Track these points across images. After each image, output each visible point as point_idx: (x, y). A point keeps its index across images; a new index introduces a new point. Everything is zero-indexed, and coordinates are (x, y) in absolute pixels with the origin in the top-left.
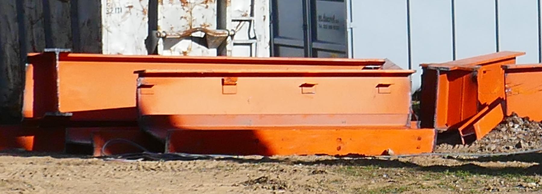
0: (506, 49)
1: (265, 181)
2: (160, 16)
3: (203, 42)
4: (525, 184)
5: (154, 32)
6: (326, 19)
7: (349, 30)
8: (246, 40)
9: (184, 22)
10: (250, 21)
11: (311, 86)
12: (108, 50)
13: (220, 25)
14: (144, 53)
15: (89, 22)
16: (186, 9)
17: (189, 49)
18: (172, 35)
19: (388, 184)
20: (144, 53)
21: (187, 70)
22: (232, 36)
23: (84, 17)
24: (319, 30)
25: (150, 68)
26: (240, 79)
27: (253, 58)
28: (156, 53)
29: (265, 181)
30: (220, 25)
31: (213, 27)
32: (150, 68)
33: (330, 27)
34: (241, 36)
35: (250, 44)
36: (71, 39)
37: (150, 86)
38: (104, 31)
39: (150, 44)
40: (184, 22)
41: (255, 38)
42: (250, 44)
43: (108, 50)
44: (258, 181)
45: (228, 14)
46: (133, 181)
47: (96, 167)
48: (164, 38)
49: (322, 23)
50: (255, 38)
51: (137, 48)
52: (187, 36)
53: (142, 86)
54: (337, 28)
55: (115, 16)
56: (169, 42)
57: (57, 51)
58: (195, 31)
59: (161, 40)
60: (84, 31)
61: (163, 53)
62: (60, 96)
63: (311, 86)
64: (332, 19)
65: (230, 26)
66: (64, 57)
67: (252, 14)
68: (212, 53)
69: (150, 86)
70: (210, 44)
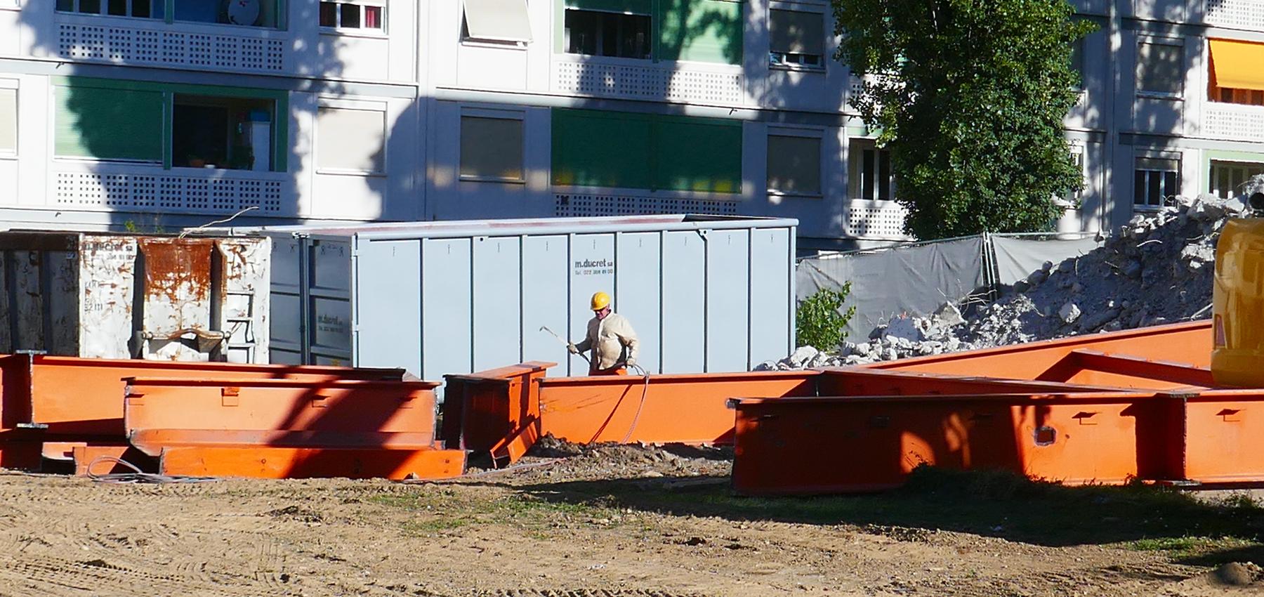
0: (531, 358)
1: (295, 512)
2: (146, 314)
3: (194, 344)
4: (595, 521)
5: (139, 333)
6: (327, 320)
7: (354, 334)
8: (242, 343)
9: (173, 322)
10: (248, 322)
11: (1089, 415)
12: (84, 355)
13: (214, 324)
14: (126, 356)
15: (63, 320)
16: (176, 306)
17: (178, 353)
18: (160, 336)
19: (437, 517)
20: (126, 356)
21: (175, 378)
22: (227, 339)
23: (57, 314)
24: (318, 332)
25: (141, 374)
26: (242, 389)
27: (251, 364)
28: (141, 356)
29: (295, 512)
30: (214, 324)
31: (205, 328)
32: (141, 374)
33: (332, 330)
34: (238, 339)
35: (247, 349)
36: (41, 339)
37: (140, 396)
38: (82, 330)
39: (134, 346)
40: (173, 322)
41: (253, 341)
42: (247, 349)
43: (84, 355)
44: (286, 511)
45: (223, 313)
46: (136, 507)
47: (87, 489)
48: (150, 340)
49: (323, 325)
50: (253, 341)
51: (119, 350)
52: (177, 338)
53: (131, 396)
54: (341, 331)
55: (94, 313)
56: (156, 344)
57: (31, 353)
58: (186, 332)
59: (146, 342)
60: (57, 331)
61: (148, 357)
62: (33, 405)
63: (1089, 415)
64: (335, 320)
65: (225, 327)
66: (39, 360)
67: (250, 315)
68: (203, 358)
69: (140, 396)
70: (202, 347)
